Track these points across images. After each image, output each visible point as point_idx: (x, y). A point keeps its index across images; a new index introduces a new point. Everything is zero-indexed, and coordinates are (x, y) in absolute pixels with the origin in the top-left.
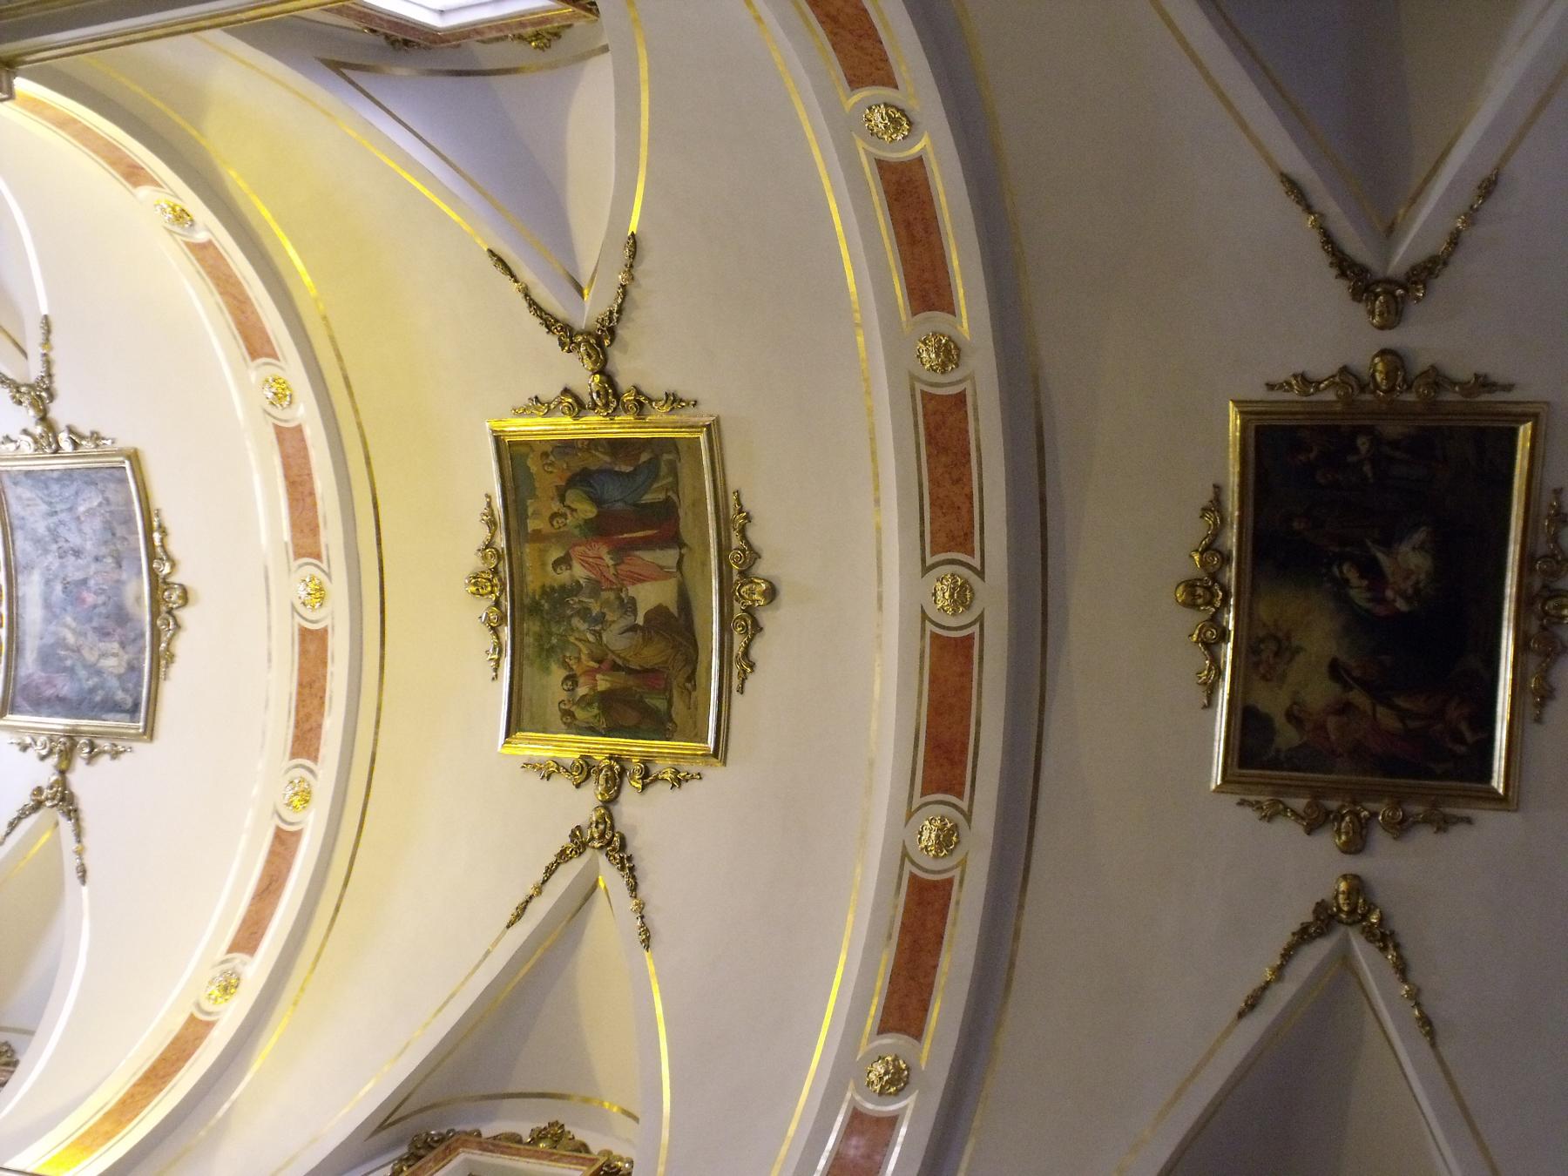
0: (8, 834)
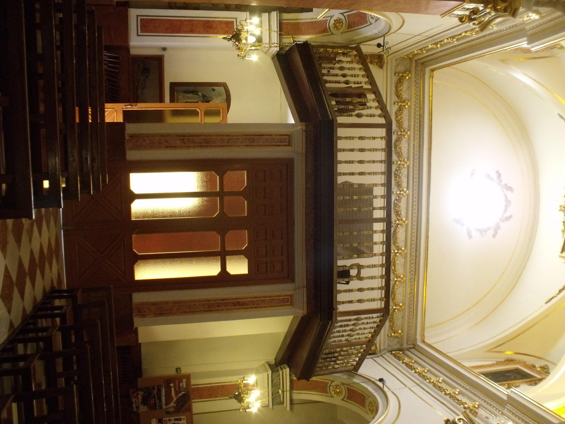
0: (558, 294)
